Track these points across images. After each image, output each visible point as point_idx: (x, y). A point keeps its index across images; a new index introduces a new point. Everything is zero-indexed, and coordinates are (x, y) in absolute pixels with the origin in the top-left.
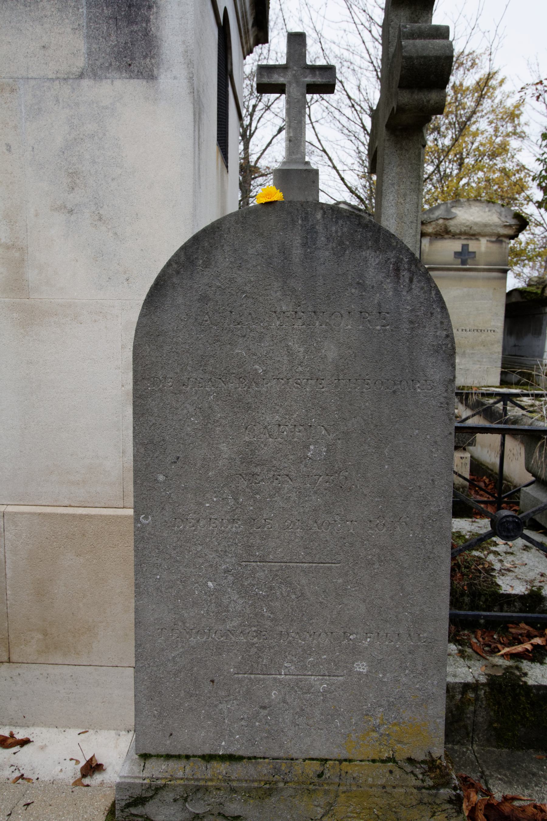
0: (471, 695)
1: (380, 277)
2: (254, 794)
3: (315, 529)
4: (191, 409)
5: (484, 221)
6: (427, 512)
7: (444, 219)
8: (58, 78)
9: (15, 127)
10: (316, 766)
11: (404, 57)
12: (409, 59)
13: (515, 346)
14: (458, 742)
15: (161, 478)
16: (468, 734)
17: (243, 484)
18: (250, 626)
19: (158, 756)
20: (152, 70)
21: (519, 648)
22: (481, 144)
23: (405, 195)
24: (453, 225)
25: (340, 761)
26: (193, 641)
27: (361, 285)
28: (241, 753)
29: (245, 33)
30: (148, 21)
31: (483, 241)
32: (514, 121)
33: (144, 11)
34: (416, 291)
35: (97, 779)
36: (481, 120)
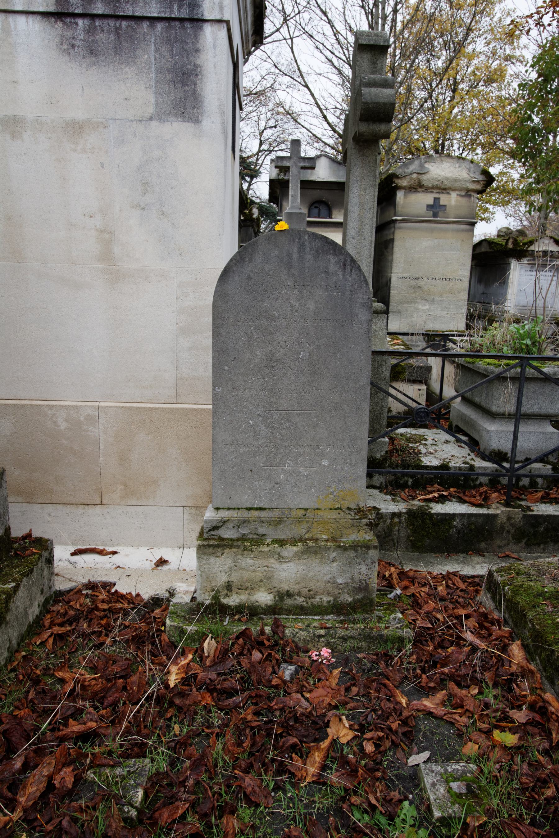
0: (396, 520)
1: (336, 268)
2: (272, 523)
3: (303, 394)
4: (242, 334)
5: (454, 177)
6: (358, 386)
7: (418, 173)
8: (135, 120)
9: (107, 152)
10: (303, 512)
11: (363, 103)
12: (367, 103)
13: (483, 293)
14: (388, 550)
15: (226, 368)
16: (394, 544)
17: (268, 371)
18: (270, 443)
19: (224, 509)
20: (198, 117)
21: (430, 496)
22: (477, 69)
23: (365, 189)
24: (426, 180)
25: (314, 509)
26: (242, 450)
27: (327, 273)
28: (265, 507)
29: (246, 43)
30: (195, 84)
31: (454, 195)
32: (513, 43)
33: (193, 78)
34: (354, 276)
35: (165, 568)
36: (478, 40)
